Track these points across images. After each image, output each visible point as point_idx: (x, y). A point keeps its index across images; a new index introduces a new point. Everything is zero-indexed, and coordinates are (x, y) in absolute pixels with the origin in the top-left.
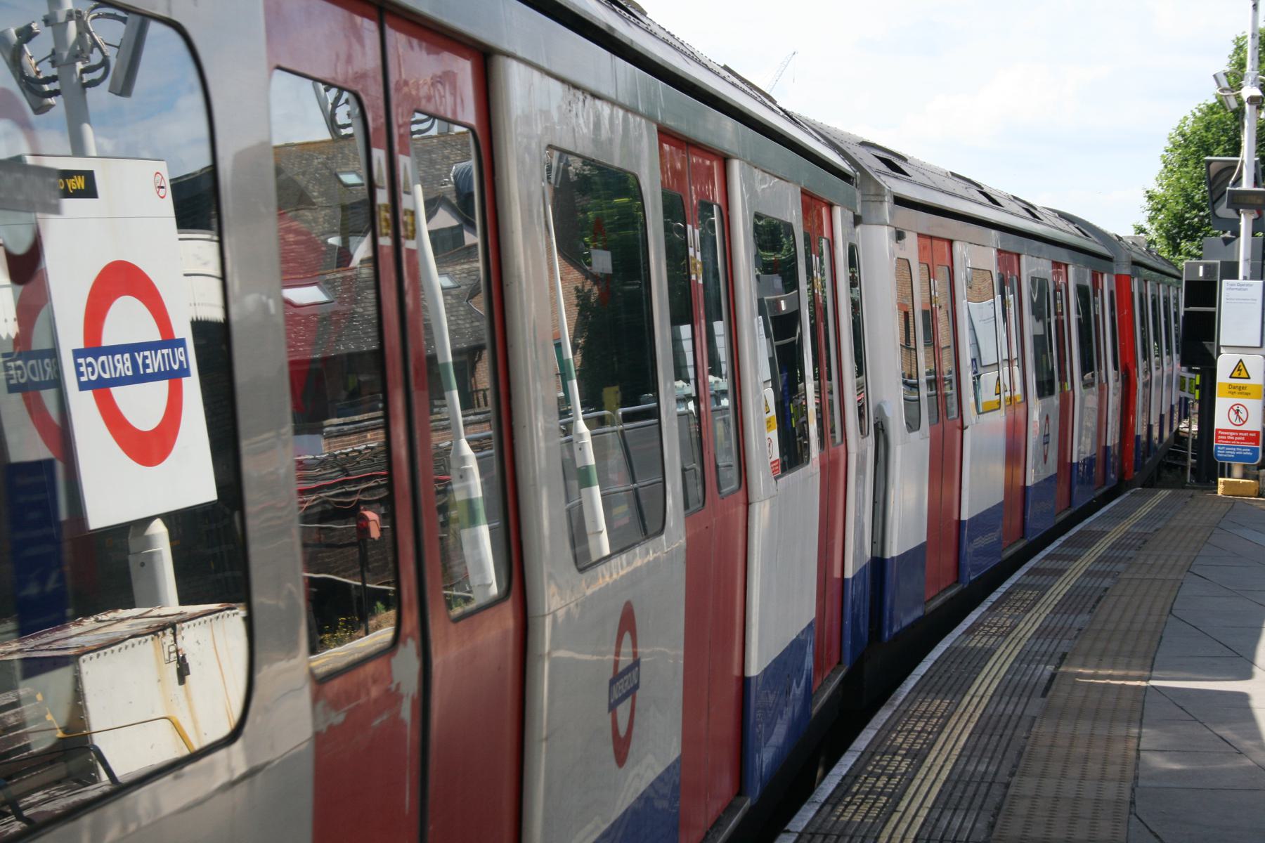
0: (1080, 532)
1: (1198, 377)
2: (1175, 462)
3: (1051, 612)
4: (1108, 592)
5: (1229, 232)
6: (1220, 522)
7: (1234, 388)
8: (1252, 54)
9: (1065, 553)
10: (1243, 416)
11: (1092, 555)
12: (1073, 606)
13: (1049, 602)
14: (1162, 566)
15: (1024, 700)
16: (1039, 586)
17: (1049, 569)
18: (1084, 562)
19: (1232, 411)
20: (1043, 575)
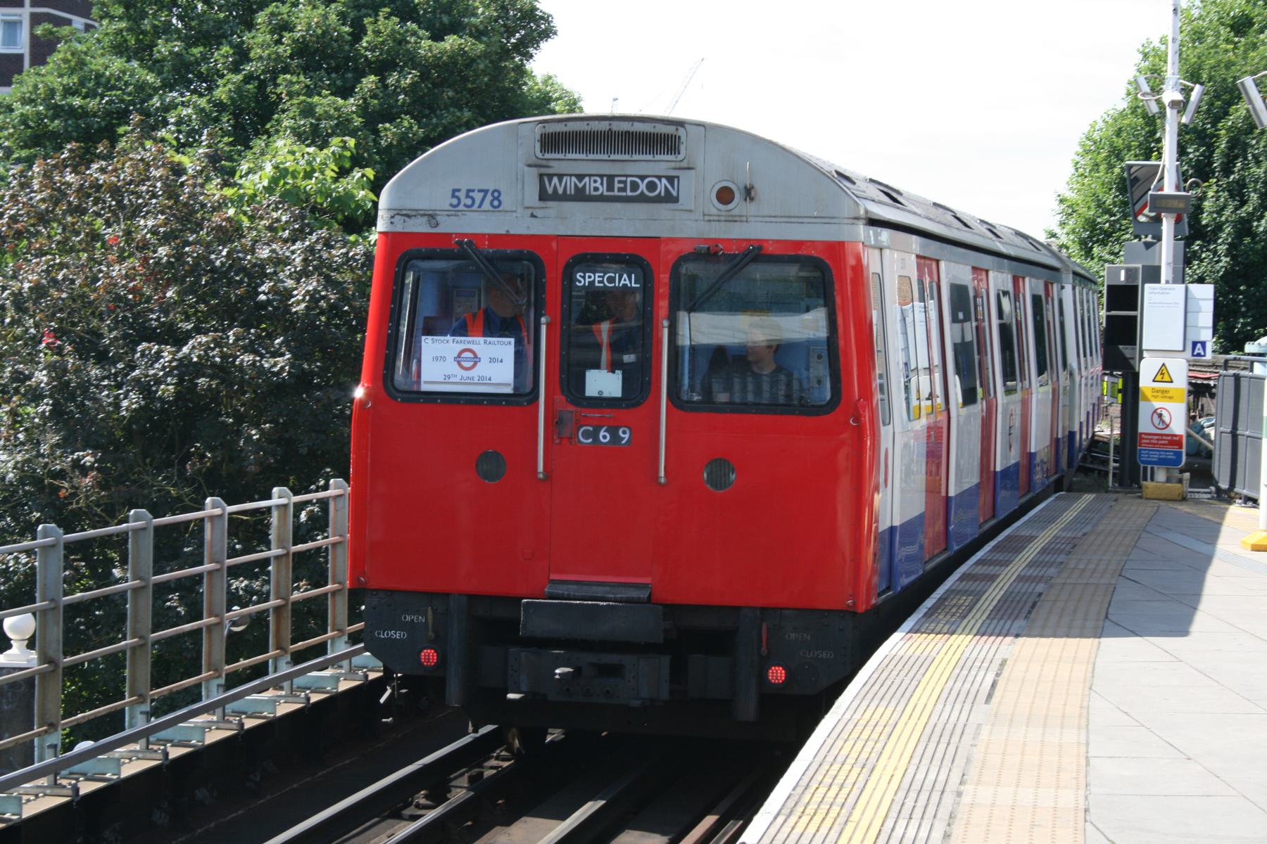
0: (1008, 537)
1: (1120, 381)
2: (1091, 466)
3: (987, 618)
4: (1043, 597)
5: (1150, 236)
6: (1147, 525)
7: (1158, 391)
8: (1173, 57)
9: (995, 558)
11: (1023, 560)
12: (1009, 612)
13: (984, 607)
14: (1094, 571)
15: (967, 707)
16: (973, 591)
17: (981, 575)
18: (1016, 567)
20: (976, 580)
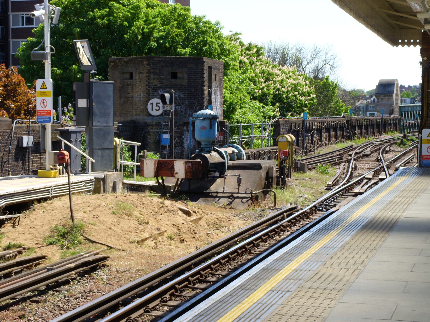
7: (42, 93)
10: (45, 104)
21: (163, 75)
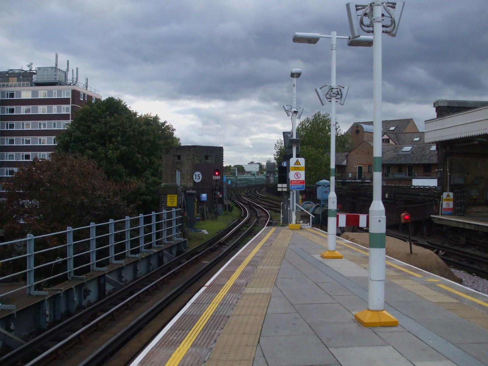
10: (299, 176)
19: (295, 175)
21: (201, 157)
